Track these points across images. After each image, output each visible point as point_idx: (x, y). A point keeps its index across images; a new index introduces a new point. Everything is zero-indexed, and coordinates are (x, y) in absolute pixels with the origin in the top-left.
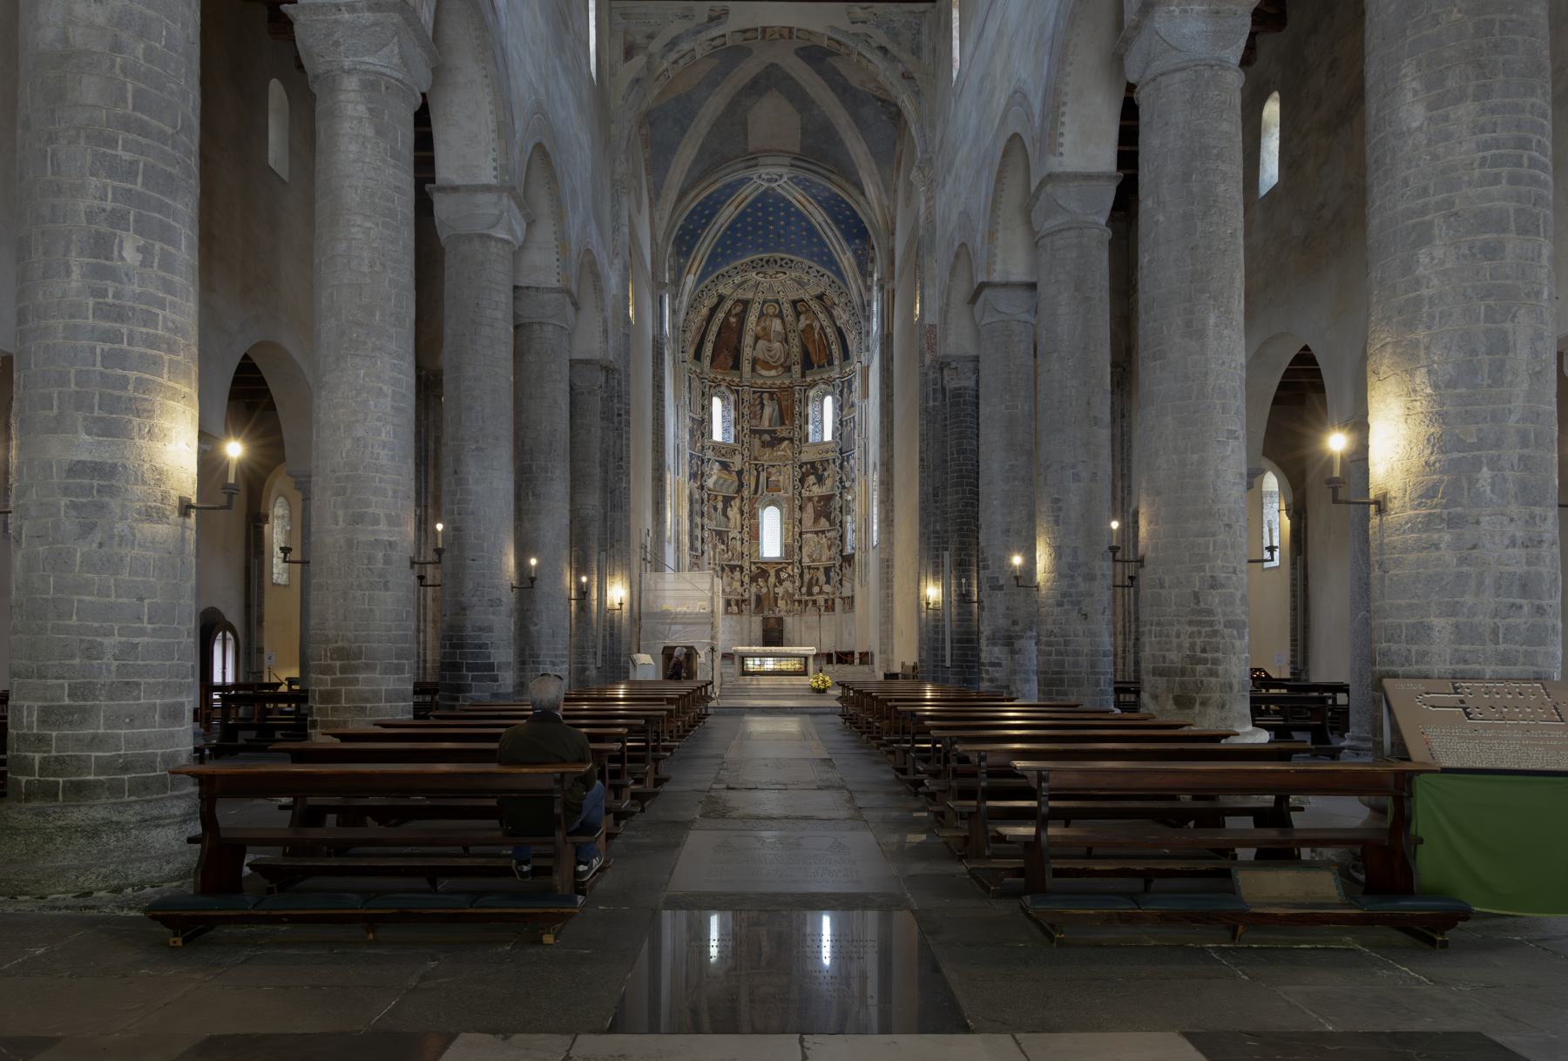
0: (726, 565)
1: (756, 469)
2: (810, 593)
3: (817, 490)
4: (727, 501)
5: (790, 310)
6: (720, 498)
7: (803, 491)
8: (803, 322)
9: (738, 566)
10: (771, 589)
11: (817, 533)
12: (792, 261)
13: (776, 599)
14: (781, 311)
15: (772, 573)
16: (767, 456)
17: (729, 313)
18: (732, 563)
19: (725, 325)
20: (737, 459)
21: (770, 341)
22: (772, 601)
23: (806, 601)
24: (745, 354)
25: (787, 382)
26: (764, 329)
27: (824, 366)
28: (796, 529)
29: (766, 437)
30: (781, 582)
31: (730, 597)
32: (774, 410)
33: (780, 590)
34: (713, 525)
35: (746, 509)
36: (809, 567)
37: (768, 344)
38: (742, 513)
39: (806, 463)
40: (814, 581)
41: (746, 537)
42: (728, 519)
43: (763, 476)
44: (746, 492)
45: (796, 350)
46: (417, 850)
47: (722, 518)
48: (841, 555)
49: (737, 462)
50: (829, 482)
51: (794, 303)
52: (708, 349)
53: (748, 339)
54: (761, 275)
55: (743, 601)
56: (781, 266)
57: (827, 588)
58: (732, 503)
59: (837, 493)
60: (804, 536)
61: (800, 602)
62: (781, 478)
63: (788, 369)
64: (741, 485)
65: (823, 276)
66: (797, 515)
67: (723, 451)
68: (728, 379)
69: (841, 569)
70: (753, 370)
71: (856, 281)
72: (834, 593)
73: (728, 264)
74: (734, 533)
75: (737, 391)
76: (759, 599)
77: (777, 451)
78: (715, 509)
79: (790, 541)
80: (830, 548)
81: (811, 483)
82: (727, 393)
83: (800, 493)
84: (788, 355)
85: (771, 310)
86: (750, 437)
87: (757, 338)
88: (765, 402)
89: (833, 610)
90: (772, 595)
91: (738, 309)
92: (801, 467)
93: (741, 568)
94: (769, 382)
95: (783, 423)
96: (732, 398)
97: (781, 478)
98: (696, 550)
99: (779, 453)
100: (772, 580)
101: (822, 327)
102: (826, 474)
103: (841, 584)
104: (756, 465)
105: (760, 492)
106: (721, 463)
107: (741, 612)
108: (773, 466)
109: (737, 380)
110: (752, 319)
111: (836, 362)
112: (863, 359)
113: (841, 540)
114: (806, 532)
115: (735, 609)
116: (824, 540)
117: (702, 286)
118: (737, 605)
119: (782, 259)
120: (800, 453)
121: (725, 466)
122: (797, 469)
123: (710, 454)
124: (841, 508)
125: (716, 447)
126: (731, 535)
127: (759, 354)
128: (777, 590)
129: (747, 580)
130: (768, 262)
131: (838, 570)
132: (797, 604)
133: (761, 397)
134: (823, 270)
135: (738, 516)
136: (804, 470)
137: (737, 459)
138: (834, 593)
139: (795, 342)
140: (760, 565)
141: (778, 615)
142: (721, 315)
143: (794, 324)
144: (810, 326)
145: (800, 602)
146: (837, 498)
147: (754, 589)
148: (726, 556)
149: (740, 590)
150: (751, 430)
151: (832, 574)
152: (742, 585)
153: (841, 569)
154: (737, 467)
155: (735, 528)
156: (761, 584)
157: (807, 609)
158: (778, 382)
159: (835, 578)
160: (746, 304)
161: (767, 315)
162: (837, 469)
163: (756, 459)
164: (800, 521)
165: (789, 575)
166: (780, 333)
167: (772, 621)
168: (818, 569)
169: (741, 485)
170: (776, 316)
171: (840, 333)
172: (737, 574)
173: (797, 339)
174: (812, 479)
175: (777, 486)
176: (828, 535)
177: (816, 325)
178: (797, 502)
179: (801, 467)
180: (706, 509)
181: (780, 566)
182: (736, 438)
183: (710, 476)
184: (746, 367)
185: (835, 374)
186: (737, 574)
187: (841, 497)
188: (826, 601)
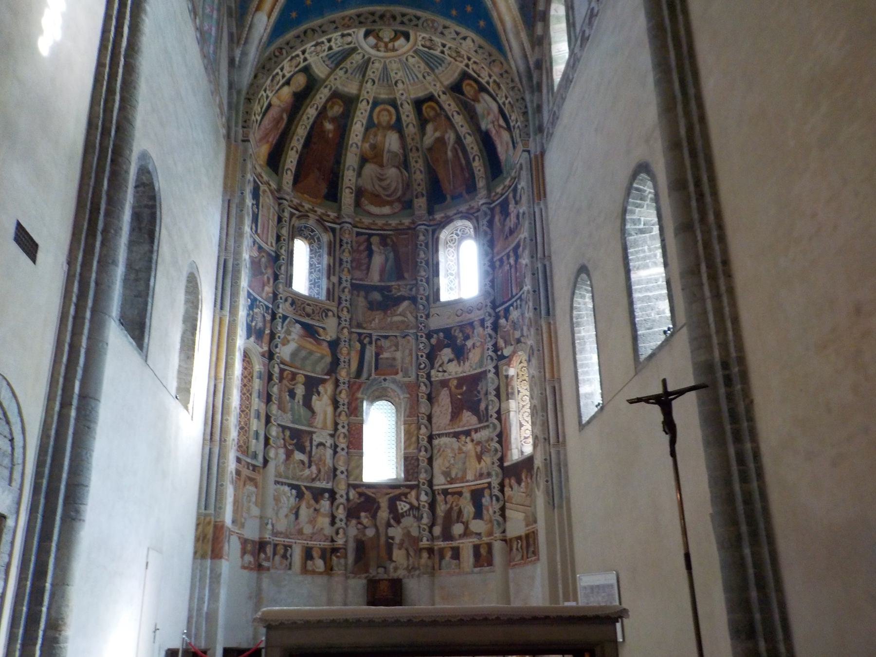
0: (307, 488)
1: (360, 341)
2: (447, 535)
3: (455, 370)
4: (312, 385)
5: (412, 116)
6: (301, 379)
7: (433, 372)
8: (431, 134)
9: (324, 490)
10: (382, 530)
11: (456, 435)
12: (418, 18)
13: (389, 548)
14: (399, 119)
15: (384, 503)
16: (375, 324)
17: (322, 114)
18: (318, 484)
19: (315, 131)
20: (331, 324)
21: (381, 166)
22: (383, 553)
23: (442, 551)
24: (346, 180)
25: (407, 222)
26: (374, 147)
27: (461, 195)
28: (423, 430)
29: (376, 296)
30: (397, 517)
31: (311, 543)
32: (387, 260)
33: (396, 532)
34: (286, 420)
35: (343, 397)
36: (445, 492)
37: (378, 170)
38: (335, 404)
39: (437, 332)
40: (454, 515)
41: (342, 443)
42: (313, 412)
43: (370, 352)
44: (343, 373)
45: (420, 178)
46: (547, 366)
47: (303, 411)
48: (501, 466)
49: (330, 328)
50: (474, 356)
51: (418, 104)
52: (291, 160)
53: (351, 159)
54: (372, 40)
55: (334, 550)
56: (402, 23)
57: (477, 526)
58: (321, 389)
59: (491, 367)
60: (436, 442)
61: (430, 551)
62: (398, 355)
63: (408, 206)
64: (335, 363)
65: (465, 38)
66: (424, 409)
67: (309, 310)
68: (320, 211)
69: (502, 491)
70: (358, 204)
71: (517, 34)
72: (490, 534)
73: (321, 14)
74: (322, 436)
75: (333, 230)
76: (361, 547)
77: (393, 315)
78: (292, 394)
79: (412, 450)
80: (479, 458)
81: (446, 359)
82: (318, 231)
83: (429, 376)
84: (408, 186)
85: (384, 118)
86: (351, 292)
87: (364, 160)
88: (374, 248)
89: (490, 563)
90: (383, 539)
91: (337, 110)
92: (429, 336)
93: (333, 494)
94: (380, 222)
95: (401, 277)
96: (325, 238)
97: (398, 355)
98: (255, 456)
99: (396, 319)
100: (384, 514)
101: (459, 140)
102: (469, 343)
103: (503, 515)
104: (360, 334)
105: (365, 375)
106: (304, 326)
107: (329, 570)
108: (386, 337)
109: (333, 215)
110: (357, 128)
111: (481, 184)
112: (532, 147)
113: (500, 442)
114: (439, 435)
115: (319, 564)
116: (470, 446)
117: (280, 42)
118: (323, 557)
119: (403, 15)
120: (428, 316)
121: (310, 331)
122: (424, 339)
123: (284, 309)
124: (498, 390)
125: (297, 301)
126: (317, 439)
127: (366, 182)
128: (392, 532)
129: (341, 513)
130: (382, 17)
131: (496, 492)
132: (425, 555)
133: (368, 241)
134: (464, 31)
135: (330, 410)
136: (434, 341)
137: (331, 324)
138: (490, 534)
139: (418, 165)
140: (363, 490)
141: (395, 575)
142: (311, 112)
143: (418, 138)
144: (441, 141)
145: (430, 551)
146: (491, 375)
147: (353, 531)
148: (307, 472)
149: (328, 531)
150: (352, 285)
151: (486, 501)
152: (333, 523)
153: (502, 491)
154: (331, 335)
155: (324, 427)
156: (365, 521)
157: (444, 563)
158: (393, 222)
159: (491, 506)
160: (350, 102)
161: (378, 126)
162: (489, 331)
163: (359, 326)
164: (430, 418)
165: (412, 507)
166: (396, 155)
167: (384, 586)
168: (460, 494)
169: (335, 363)
170: (391, 127)
171: (487, 143)
172: (325, 504)
173: (421, 162)
174: (447, 353)
175: (392, 366)
176: (476, 436)
177: (450, 137)
178: (423, 388)
179: (429, 336)
180: (275, 389)
181: (397, 492)
182: (330, 294)
183: (285, 342)
184: (347, 198)
185: (480, 200)
186: (325, 504)
187: (497, 373)
188: (476, 548)
